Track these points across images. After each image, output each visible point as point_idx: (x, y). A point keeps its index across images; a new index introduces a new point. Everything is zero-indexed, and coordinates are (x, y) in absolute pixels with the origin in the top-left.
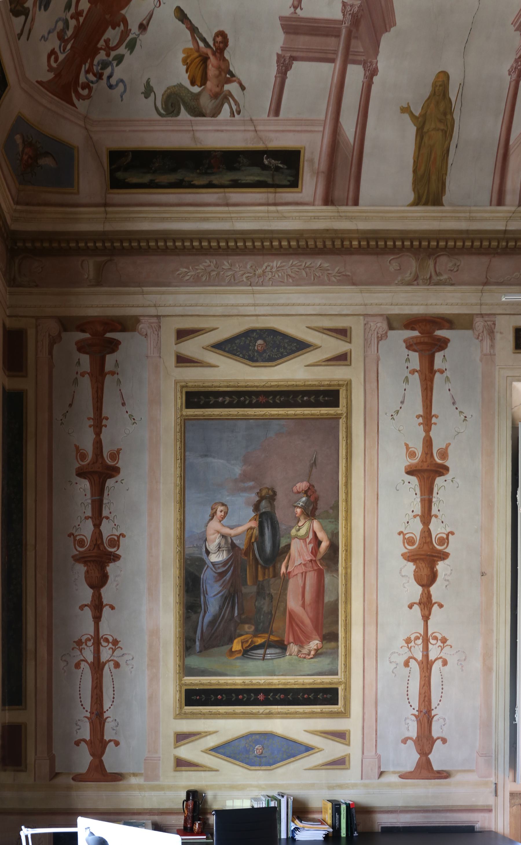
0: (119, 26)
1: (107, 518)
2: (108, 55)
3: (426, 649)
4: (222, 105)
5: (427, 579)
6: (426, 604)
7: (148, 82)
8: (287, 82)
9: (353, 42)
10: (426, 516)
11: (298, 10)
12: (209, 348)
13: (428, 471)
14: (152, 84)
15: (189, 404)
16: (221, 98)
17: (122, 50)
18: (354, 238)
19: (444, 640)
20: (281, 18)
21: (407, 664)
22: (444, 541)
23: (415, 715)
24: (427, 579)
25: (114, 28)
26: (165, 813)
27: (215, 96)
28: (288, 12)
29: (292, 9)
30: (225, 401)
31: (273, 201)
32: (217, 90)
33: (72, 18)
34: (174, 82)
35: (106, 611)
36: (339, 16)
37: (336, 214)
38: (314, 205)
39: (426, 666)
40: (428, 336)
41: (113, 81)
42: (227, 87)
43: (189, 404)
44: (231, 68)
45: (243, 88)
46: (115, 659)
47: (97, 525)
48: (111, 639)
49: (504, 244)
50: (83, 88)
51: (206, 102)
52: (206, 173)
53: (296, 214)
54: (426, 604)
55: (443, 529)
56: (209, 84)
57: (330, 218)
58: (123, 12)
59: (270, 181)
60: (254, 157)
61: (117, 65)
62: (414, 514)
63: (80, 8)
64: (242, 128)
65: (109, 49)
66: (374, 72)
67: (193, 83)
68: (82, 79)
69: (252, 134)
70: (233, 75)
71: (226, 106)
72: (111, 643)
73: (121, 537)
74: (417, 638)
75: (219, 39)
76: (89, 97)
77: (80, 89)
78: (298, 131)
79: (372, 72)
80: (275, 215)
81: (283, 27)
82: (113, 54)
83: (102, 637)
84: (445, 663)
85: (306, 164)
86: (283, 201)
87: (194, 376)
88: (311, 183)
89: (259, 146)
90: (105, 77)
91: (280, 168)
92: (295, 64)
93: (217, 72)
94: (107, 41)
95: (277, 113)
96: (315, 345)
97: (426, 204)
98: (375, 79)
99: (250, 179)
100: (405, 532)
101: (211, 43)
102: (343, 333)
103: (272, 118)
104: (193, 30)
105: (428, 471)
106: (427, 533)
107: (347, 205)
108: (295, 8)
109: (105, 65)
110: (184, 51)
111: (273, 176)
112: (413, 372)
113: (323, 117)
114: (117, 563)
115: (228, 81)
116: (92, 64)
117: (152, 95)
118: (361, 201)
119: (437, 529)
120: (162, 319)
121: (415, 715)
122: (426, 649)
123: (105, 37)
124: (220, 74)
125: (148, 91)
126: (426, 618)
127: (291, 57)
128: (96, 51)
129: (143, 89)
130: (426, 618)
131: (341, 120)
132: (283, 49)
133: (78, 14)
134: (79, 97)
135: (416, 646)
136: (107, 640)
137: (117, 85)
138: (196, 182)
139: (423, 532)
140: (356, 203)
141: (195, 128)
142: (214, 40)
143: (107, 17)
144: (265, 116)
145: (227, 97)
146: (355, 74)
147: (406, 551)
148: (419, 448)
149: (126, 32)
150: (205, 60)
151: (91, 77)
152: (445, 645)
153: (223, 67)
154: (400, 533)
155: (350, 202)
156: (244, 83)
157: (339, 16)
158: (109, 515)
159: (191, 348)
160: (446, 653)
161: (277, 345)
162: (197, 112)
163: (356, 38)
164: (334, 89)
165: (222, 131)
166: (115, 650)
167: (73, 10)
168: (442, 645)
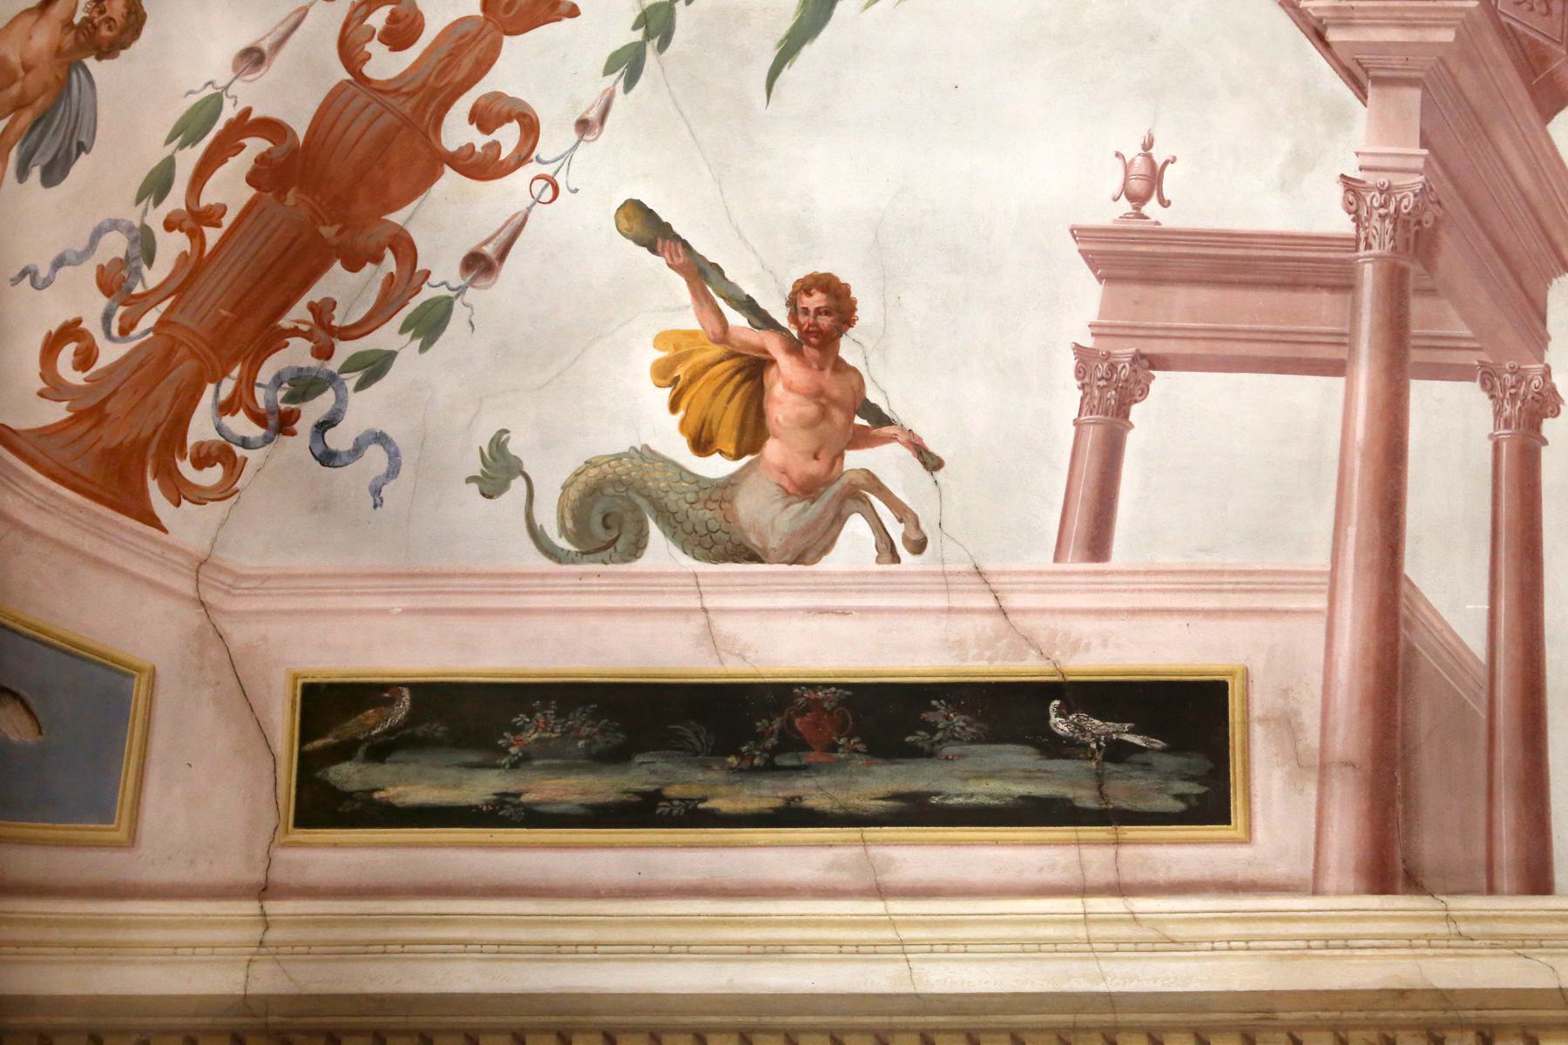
0: (377, 259)
2: (324, 353)
4: (839, 520)
7: (498, 444)
8: (1133, 443)
9: (1418, 307)
11: (1152, 208)
14: (513, 448)
16: (828, 499)
17: (387, 336)
20: (1078, 233)
25: (353, 265)
27: (808, 489)
28: (1110, 212)
29: (1125, 206)
31: (1110, 877)
32: (815, 468)
33: (169, 225)
34: (619, 442)
36: (1340, 223)
37: (1441, 929)
38: (1316, 892)
41: (338, 439)
42: (855, 460)
44: (872, 396)
45: (932, 463)
50: (201, 462)
51: (761, 509)
52: (770, 768)
53: (1226, 929)
56: (773, 450)
57: (1410, 942)
58: (397, 217)
59: (1086, 798)
60: (1008, 710)
61: (360, 386)
63: (209, 197)
64: (939, 601)
65: (325, 333)
66: (1544, 403)
67: (702, 445)
68: (202, 427)
69: (989, 624)
70: (879, 418)
75: (816, 300)
76: (225, 491)
77: (185, 468)
78: (1208, 613)
79: (1528, 415)
80: (1124, 931)
81: (1092, 259)
82: (345, 350)
85: (1258, 732)
86: (1161, 876)
88: (1285, 806)
89: (1029, 667)
90: (304, 426)
92: (1161, 381)
93: (811, 410)
94: (322, 311)
95: (1098, 544)
98: (1549, 427)
99: (984, 791)
101: (781, 315)
103: (1073, 565)
104: (701, 274)
107: (1491, 890)
108: (1138, 200)
109: (305, 386)
110: (661, 340)
111: (1100, 779)
113: (1320, 560)
115: (860, 439)
116: (248, 382)
117: (518, 485)
118: (1562, 875)
123: (316, 293)
124: (824, 414)
125: (499, 470)
127: (1138, 358)
128: (274, 340)
129: (476, 468)
131: (1409, 569)
132: (1098, 330)
133: (195, 219)
134: (179, 491)
137: (357, 451)
138: (723, 805)
140: (1538, 880)
141: (711, 602)
142: (792, 302)
143: (328, 232)
144: (1045, 560)
145: (860, 493)
146: (1451, 423)
149: (410, 276)
150: (755, 368)
151: (240, 424)
153: (835, 392)
155: (1505, 879)
156: (932, 446)
157: (1340, 223)
162: (727, 545)
163: (1432, 292)
164: (1356, 464)
165: (844, 612)
167: (176, 199)
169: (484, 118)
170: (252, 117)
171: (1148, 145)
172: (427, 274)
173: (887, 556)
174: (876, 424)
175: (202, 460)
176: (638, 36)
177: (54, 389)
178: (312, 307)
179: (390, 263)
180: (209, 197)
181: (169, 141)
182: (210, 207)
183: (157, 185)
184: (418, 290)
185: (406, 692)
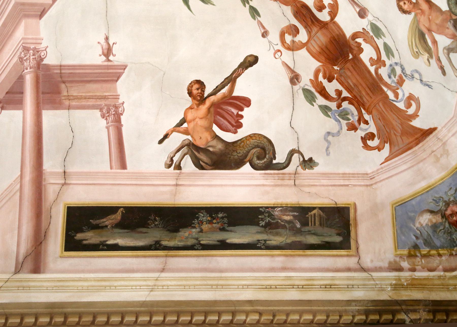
0: (360, 44)
123: (368, 64)
133: (340, 99)
169: (321, 8)
170: (313, 79)
171: (107, 39)
172: (363, 29)
173: (29, 265)
175: (409, 106)
176: (247, 6)
177: (379, 148)
178: (372, 65)
179: (359, 40)
180: (333, 94)
181: (313, 105)
182: (336, 95)
183: (325, 109)
184: (368, 32)
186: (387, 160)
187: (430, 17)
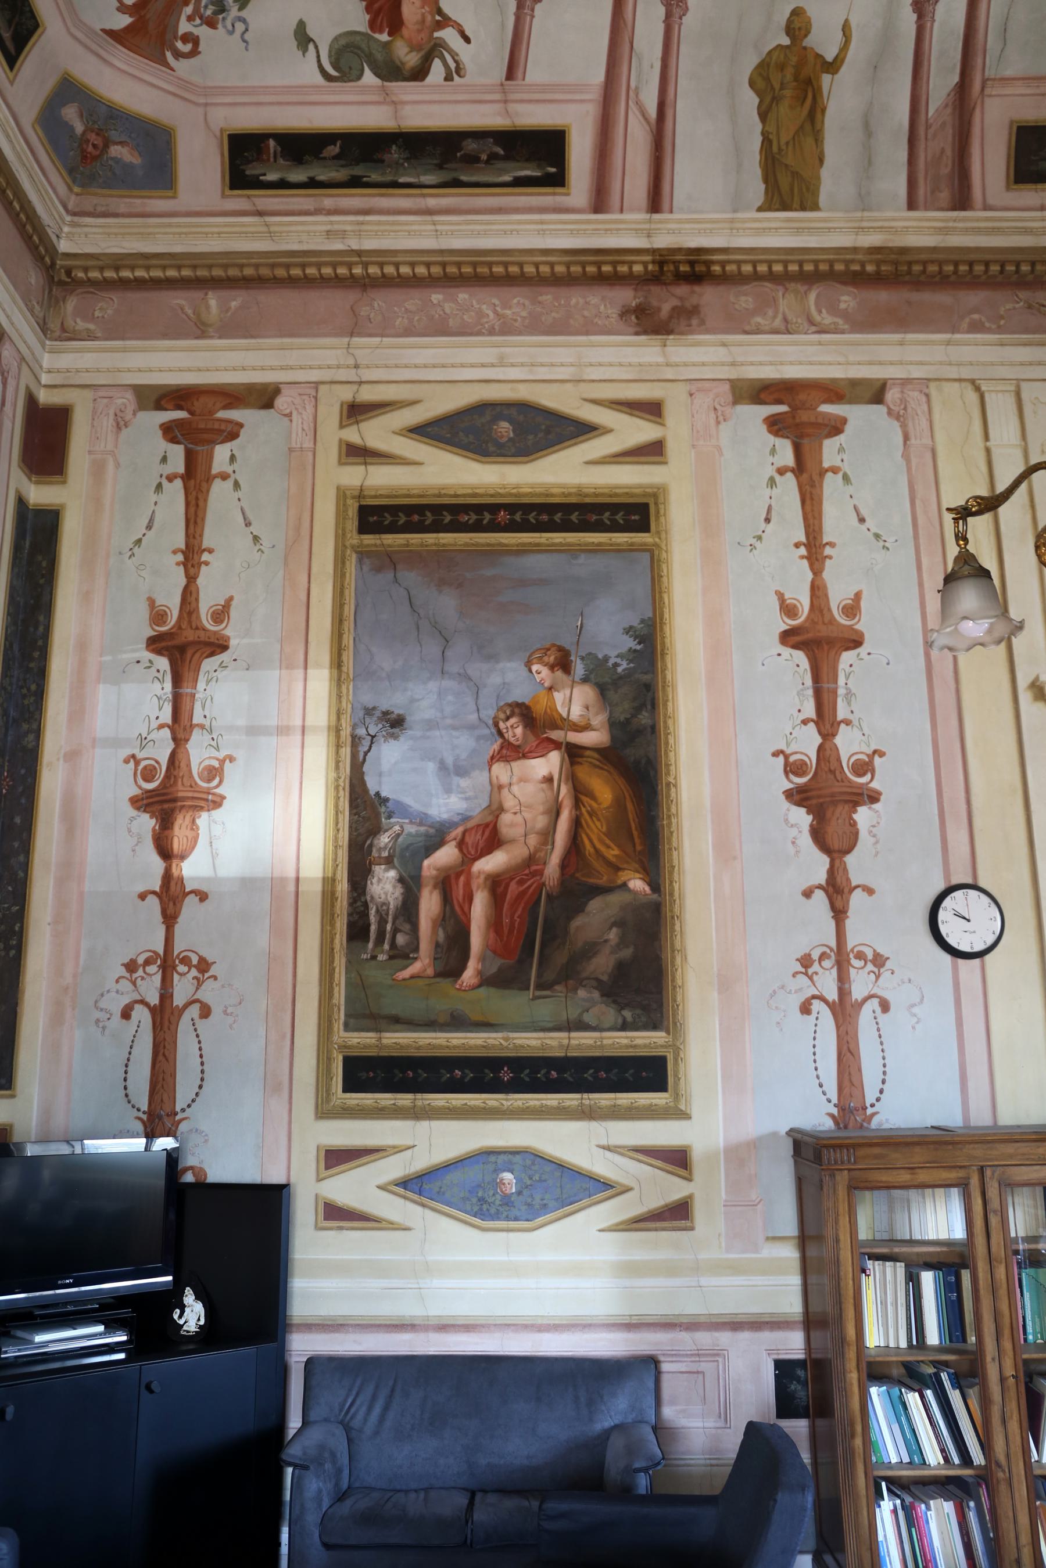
1: (848, 722)
3: (843, 979)
5: (833, 837)
6: (837, 891)
10: (825, 720)
12: (404, 432)
13: (184, 646)
15: (364, 528)
18: (947, 262)
19: (204, 966)
21: (126, 1014)
22: (864, 767)
23: (832, 1116)
24: (833, 837)
26: (453, 1326)
30: (483, 520)
35: (857, 899)
39: (844, 1010)
40: (799, 414)
43: (364, 528)
46: (880, 993)
47: (179, 740)
48: (195, 960)
49: (951, 268)
54: (837, 891)
55: (863, 745)
62: (802, 716)
68: (184, 27)
71: (437, 64)
72: (195, 966)
73: (228, 761)
74: (148, 962)
76: (194, 53)
83: (852, 950)
84: (885, 1006)
87: (382, 480)
91: (535, 156)
96: (604, 428)
97: (785, 207)
100: (788, 751)
102: (652, 410)
105: (820, 640)
106: (826, 752)
112: (781, 471)
114: (216, 814)
117: (311, 46)
119: (848, 744)
120: (323, 388)
121: (832, 1116)
122: (843, 979)
126: (839, 914)
130: (839, 914)
134: (178, 55)
135: (148, 978)
136: (186, 961)
139: (821, 749)
147: (791, 786)
148: (172, 603)
152: (206, 975)
154: (776, 754)
156: (468, 33)
158: (850, 717)
159: (374, 433)
160: (887, 986)
161: (541, 429)
166: (203, 982)
168: (876, 970)
174: (445, 21)
185: (272, 143)
186: (112, 34)
187: (484, 157)
